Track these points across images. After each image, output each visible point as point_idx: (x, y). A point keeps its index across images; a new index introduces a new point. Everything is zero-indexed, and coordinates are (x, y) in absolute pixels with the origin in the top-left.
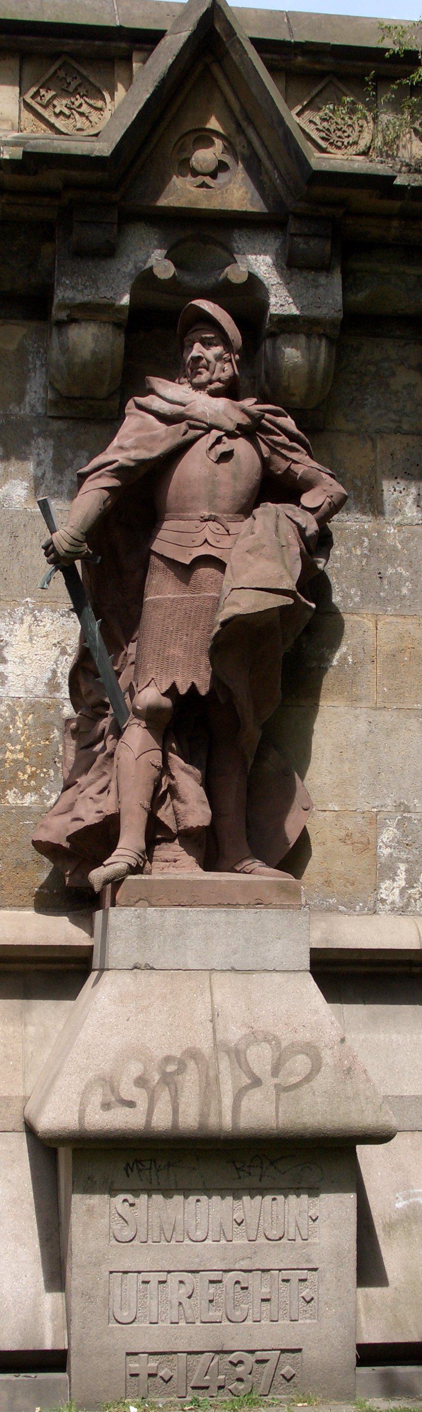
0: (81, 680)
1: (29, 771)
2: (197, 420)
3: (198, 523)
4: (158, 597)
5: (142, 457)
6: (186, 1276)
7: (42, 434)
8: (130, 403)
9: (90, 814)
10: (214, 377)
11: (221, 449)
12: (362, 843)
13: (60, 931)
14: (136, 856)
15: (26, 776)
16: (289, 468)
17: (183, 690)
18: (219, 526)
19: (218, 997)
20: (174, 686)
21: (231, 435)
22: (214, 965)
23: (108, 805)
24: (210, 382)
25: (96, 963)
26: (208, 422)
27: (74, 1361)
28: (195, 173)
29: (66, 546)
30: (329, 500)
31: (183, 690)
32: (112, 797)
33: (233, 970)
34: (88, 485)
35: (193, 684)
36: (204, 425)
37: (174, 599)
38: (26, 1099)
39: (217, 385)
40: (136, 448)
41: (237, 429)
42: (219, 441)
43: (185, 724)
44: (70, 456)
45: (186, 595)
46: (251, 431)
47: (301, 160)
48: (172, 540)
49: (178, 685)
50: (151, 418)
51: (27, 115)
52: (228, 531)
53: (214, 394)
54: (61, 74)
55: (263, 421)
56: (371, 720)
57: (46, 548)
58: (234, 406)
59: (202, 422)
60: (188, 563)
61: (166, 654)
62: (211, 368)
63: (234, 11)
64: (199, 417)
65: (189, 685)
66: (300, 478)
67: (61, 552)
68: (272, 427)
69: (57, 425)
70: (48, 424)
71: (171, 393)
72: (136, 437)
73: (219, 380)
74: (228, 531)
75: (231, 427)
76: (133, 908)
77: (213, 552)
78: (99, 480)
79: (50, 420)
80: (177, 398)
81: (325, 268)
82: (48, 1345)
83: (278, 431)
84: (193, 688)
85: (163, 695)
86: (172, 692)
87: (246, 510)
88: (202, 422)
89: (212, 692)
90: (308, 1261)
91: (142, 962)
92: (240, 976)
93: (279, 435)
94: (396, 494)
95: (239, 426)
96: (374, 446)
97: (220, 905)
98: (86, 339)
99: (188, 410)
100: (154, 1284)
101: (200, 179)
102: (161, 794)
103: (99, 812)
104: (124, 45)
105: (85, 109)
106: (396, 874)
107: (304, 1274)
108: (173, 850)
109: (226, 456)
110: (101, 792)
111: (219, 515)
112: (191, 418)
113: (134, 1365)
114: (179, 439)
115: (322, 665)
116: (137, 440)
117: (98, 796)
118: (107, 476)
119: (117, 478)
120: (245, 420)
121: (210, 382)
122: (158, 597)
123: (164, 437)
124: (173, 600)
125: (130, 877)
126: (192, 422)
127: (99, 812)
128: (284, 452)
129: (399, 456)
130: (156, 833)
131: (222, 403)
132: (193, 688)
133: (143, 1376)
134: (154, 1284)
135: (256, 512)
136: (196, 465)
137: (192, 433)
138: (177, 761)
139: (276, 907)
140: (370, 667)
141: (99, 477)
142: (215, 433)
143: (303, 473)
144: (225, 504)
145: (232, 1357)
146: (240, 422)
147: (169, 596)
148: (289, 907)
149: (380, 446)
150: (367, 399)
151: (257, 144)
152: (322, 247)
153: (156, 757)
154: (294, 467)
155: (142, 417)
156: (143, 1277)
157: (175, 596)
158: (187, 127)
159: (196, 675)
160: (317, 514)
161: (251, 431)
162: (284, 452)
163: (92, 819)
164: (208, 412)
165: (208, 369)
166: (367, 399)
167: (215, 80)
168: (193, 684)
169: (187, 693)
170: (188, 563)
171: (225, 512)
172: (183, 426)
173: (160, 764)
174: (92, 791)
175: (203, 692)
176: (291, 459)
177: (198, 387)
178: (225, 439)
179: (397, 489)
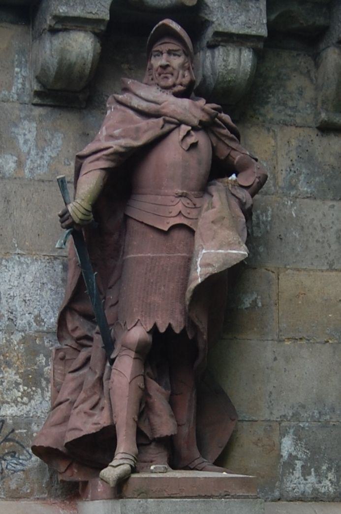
0: (69, 317)
1: (22, 390)
2: (170, 117)
3: (172, 198)
4: (140, 255)
5: (128, 145)
7: (28, 118)
8: (110, 99)
10: (178, 82)
11: (191, 140)
12: (269, 445)
14: (133, 459)
15: (20, 394)
16: (229, 154)
17: (162, 330)
18: (189, 201)
21: (194, 128)
23: (102, 419)
24: (174, 85)
26: (179, 118)
29: (80, 216)
30: (257, 180)
31: (162, 330)
34: (87, 165)
35: (170, 325)
36: (176, 121)
37: (153, 257)
39: (179, 88)
40: (124, 137)
41: (199, 124)
43: (163, 355)
44: (49, 136)
45: (163, 255)
49: (159, 325)
50: (131, 112)
52: (195, 205)
53: (178, 95)
55: (216, 119)
56: (275, 350)
57: (61, 216)
58: (196, 106)
59: (175, 118)
60: (166, 229)
61: (149, 301)
62: (175, 74)
64: (171, 114)
65: (167, 325)
66: (237, 162)
67: (77, 221)
68: (220, 123)
70: (31, 110)
71: (146, 93)
73: (181, 84)
74: (195, 205)
76: (137, 500)
78: (97, 163)
79: (33, 107)
80: (151, 97)
83: (224, 126)
84: (170, 328)
85: (148, 332)
86: (154, 331)
87: (204, 189)
88: (175, 118)
93: (224, 128)
94: (292, 173)
95: (201, 122)
97: (200, 497)
99: (163, 108)
103: (95, 424)
106: (294, 469)
108: (153, 451)
109: (194, 146)
111: (189, 193)
112: (165, 115)
114: (157, 132)
115: (239, 307)
116: (124, 130)
117: (91, 411)
118: (104, 159)
119: (112, 161)
120: (205, 118)
121: (174, 85)
122: (140, 255)
124: (152, 258)
126: (167, 118)
127: (95, 424)
128: (227, 141)
129: (293, 143)
130: (143, 440)
131: (186, 102)
135: (213, 189)
136: (172, 152)
137: (168, 127)
139: (239, 497)
140: (274, 308)
141: (98, 159)
142: (184, 128)
143: (240, 159)
146: (201, 118)
147: (149, 254)
148: (247, 497)
150: (270, 97)
154: (233, 153)
155: (124, 112)
157: (155, 255)
159: (170, 318)
160: (251, 189)
162: (227, 141)
163: (89, 428)
164: (179, 110)
165: (172, 74)
166: (270, 97)
168: (170, 325)
169: (165, 332)
170: (166, 229)
171: (193, 190)
172: (160, 121)
173: (143, 387)
174: (86, 406)
176: (231, 147)
177: (165, 88)
178: (192, 132)
179: (292, 169)
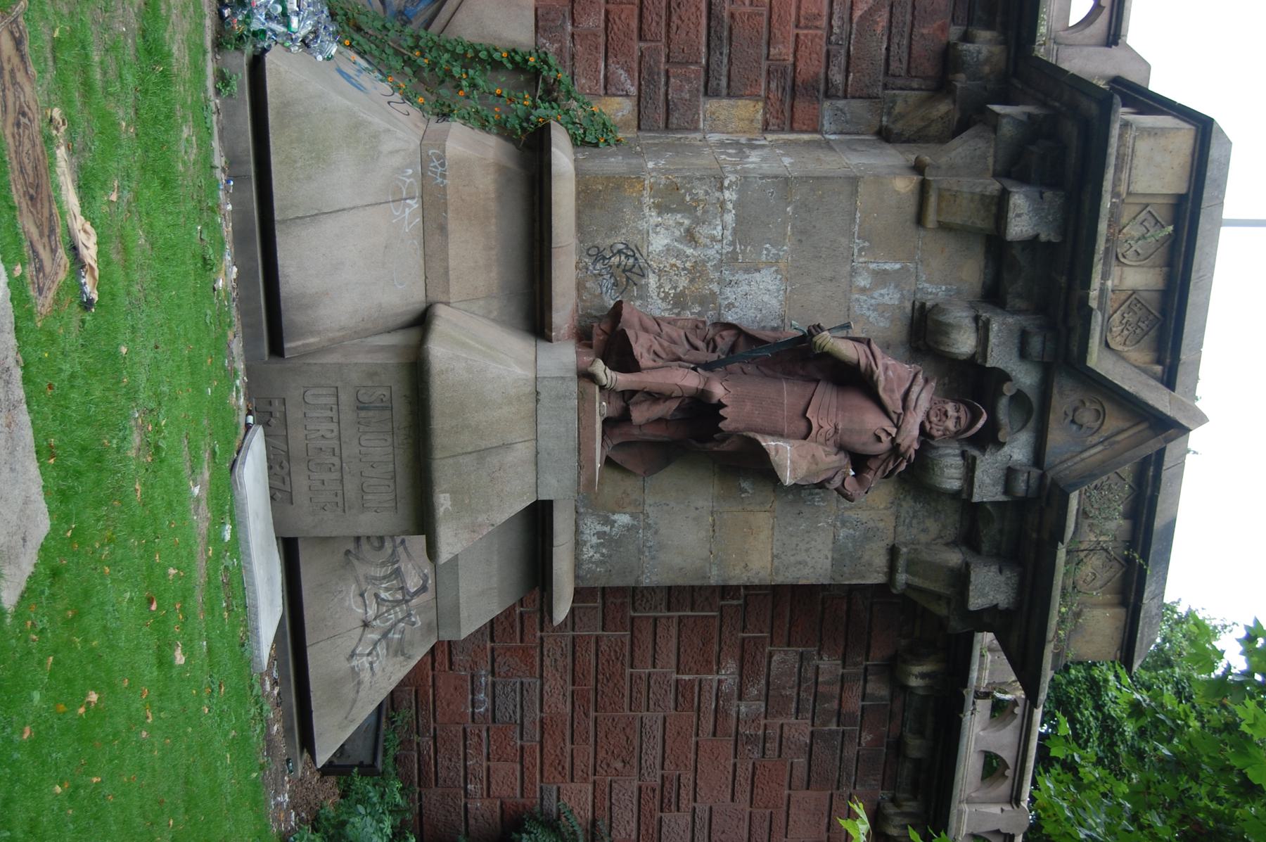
0: (733, 332)
6: (336, 433)
9: (641, 347)
11: (883, 436)
13: (563, 313)
17: (722, 412)
19: (519, 446)
20: (724, 406)
21: (893, 440)
22: (541, 442)
25: (543, 345)
27: (276, 365)
28: (1075, 410)
31: (722, 412)
32: (651, 364)
33: (537, 453)
34: (862, 348)
38: (447, 304)
42: (889, 434)
43: (700, 412)
46: (895, 450)
47: (1075, 486)
48: (825, 396)
49: (726, 422)
51: (1123, 297)
53: (922, 425)
54: (1151, 317)
63: (1181, 439)
69: (908, 306)
71: (923, 398)
72: (893, 372)
75: (899, 441)
77: (814, 432)
80: (920, 402)
81: (1007, 490)
82: (287, 345)
84: (724, 418)
86: (721, 405)
87: (842, 448)
89: (720, 430)
90: (350, 508)
91: (541, 397)
92: (533, 459)
95: (899, 445)
96: (886, 508)
97: (579, 444)
98: (964, 343)
100: (329, 414)
101: (1071, 414)
102: (655, 396)
104: (1168, 361)
105: (1126, 332)
107: (340, 504)
109: (879, 439)
110: (655, 353)
113: (276, 403)
114: (891, 408)
120: (902, 449)
123: (893, 400)
125: (597, 388)
130: (628, 395)
131: (916, 432)
132: (724, 418)
133: (271, 409)
134: (329, 414)
135: (842, 455)
136: (873, 420)
137: (894, 417)
138: (674, 405)
142: (893, 431)
144: (846, 438)
145: (285, 464)
149: (888, 512)
151: (1093, 451)
152: (1021, 487)
153: (677, 393)
154: (872, 473)
156: (335, 407)
158: (1107, 405)
159: (732, 419)
161: (895, 450)
167: (1137, 424)
174: (657, 347)
175: (720, 425)
